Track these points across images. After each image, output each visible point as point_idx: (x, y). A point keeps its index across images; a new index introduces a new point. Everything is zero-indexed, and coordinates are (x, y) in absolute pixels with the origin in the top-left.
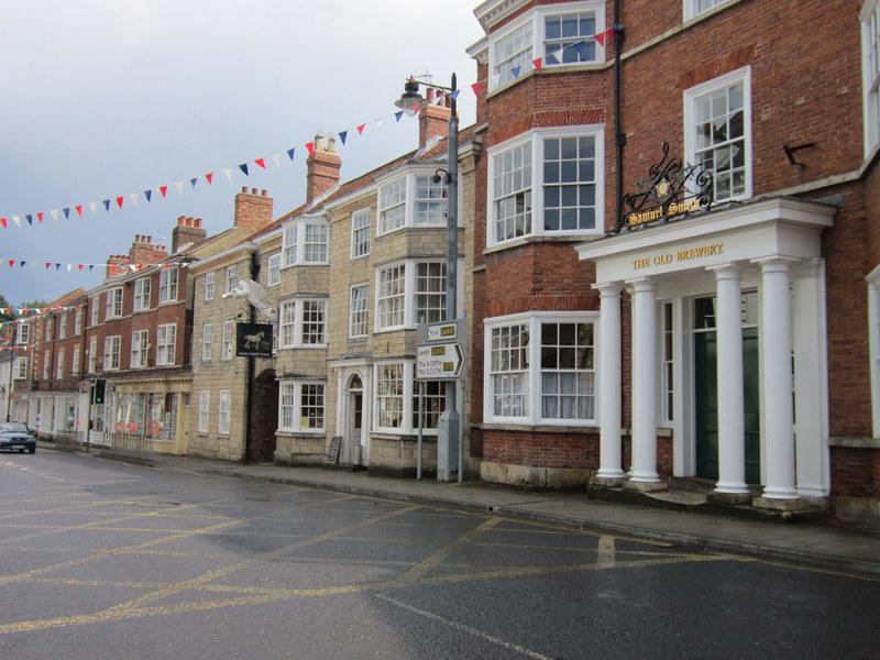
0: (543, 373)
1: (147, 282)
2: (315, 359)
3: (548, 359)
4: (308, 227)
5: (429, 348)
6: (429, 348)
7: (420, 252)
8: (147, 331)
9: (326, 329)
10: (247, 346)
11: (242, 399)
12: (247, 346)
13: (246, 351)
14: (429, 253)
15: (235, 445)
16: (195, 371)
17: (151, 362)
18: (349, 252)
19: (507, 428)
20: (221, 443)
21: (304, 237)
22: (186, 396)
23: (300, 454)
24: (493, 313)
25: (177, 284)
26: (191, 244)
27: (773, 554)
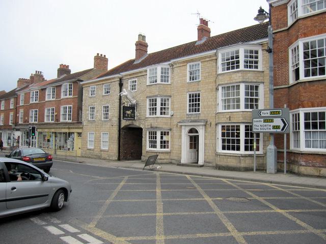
0: (305, 132)
1: (54, 89)
2: (166, 121)
3: (307, 126)
4: (162, 69)
5: (262, 120)
6: (262, 120)
7: (247, 80)
8: (72, 106)
9: (170, 110)
10: (126, 115)
11: (116, 136)
12: (126, 115)
13: (126, 117)
14: (250, 81)
15: (115, 152)
16: (85, 124)
17: (58, 120)
18: (186, 79)
19: (320, 153)
20: (102, 152)
21: (160, 73)
22: (80, 134)
23: (161, 159)
24: (292, 108)
25: (38, 96)
26: (135, 63)
27: (68, 158)
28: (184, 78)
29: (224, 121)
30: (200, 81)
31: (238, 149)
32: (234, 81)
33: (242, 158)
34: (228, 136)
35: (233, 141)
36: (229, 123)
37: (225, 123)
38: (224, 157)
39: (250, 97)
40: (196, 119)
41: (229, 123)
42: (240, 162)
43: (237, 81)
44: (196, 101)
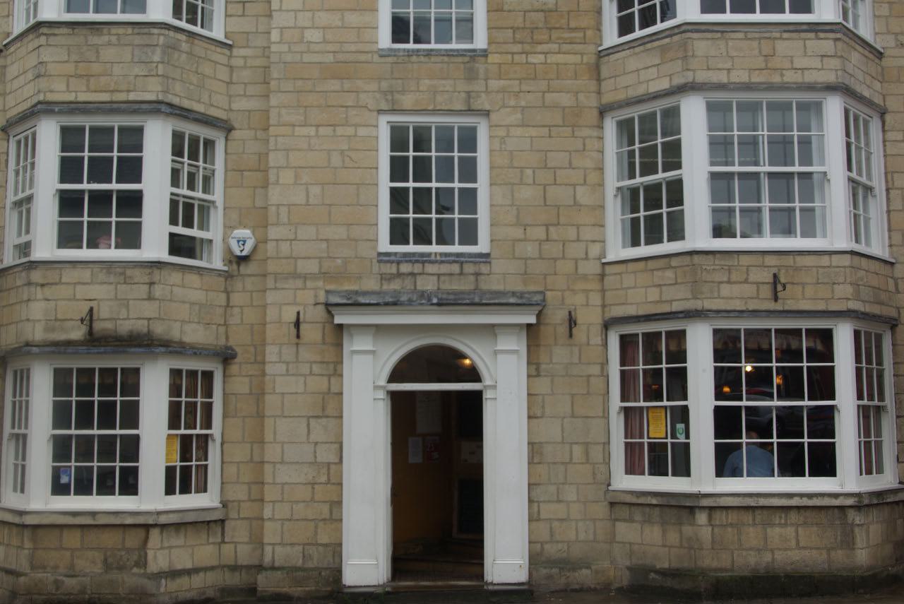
23: (174, 574)
28: (353, 19)
29: (738, 305)
30: (474, 55)
31: (825, 464)
32: (790, 77)
33: (855, 518)
34: (84, 422)
35: (107, 446)
36: (770, 313)
37: (740, 314)
38: (747, 517)
39: (411, 184)
40: (456, 286)
41: (770, 313)
42: (848, 542)
43: (810, 77)
44: (422, 174)
